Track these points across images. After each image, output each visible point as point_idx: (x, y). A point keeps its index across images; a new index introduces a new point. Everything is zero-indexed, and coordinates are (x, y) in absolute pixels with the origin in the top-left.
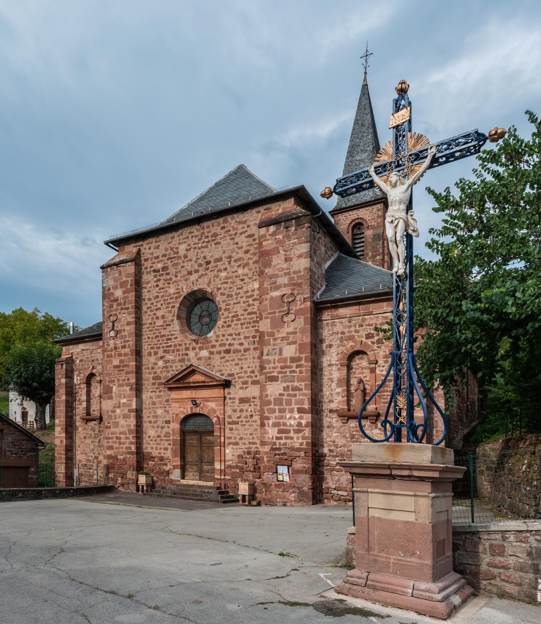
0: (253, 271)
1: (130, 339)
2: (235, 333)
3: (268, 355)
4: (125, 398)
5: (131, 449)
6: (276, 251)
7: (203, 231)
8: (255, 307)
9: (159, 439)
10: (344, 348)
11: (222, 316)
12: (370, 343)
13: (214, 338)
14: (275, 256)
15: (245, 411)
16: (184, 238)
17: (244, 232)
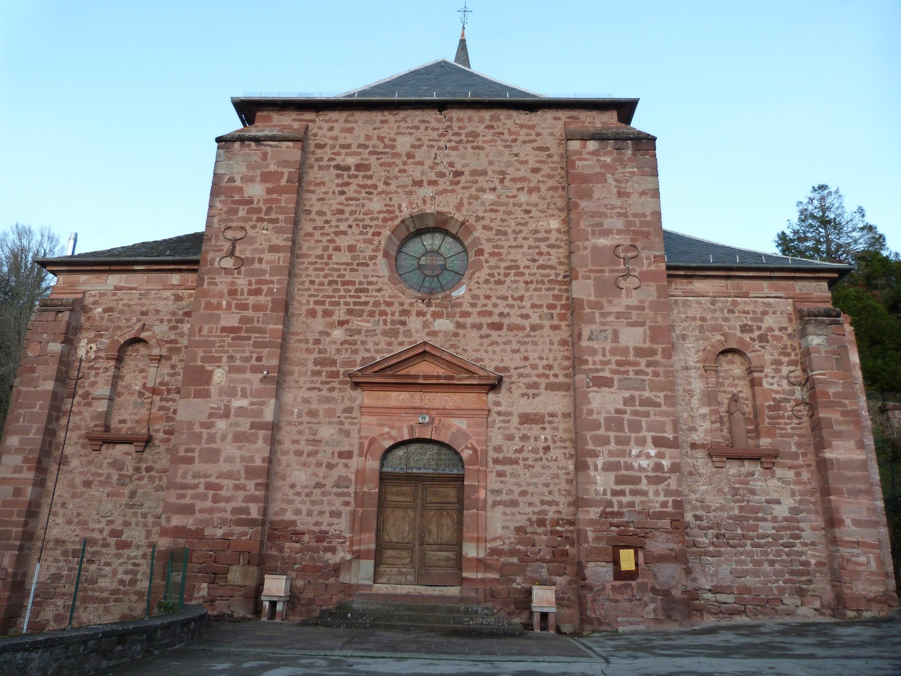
0: (548, 201)
1: (275, 279)
2: (512, 296)
3: (590, 339)
4: (244, 396)
5: (249, 513)
6: (600, 178)
7: (449, 123)
8: (553, 258)
9: (318, 491)
10: (706, 343)
11: (484, 264)
12: (748, 340)
13: (468, 299)
14: (600, 185)
15: (532, 439)
16: (408, 127)
17: (529, 142)
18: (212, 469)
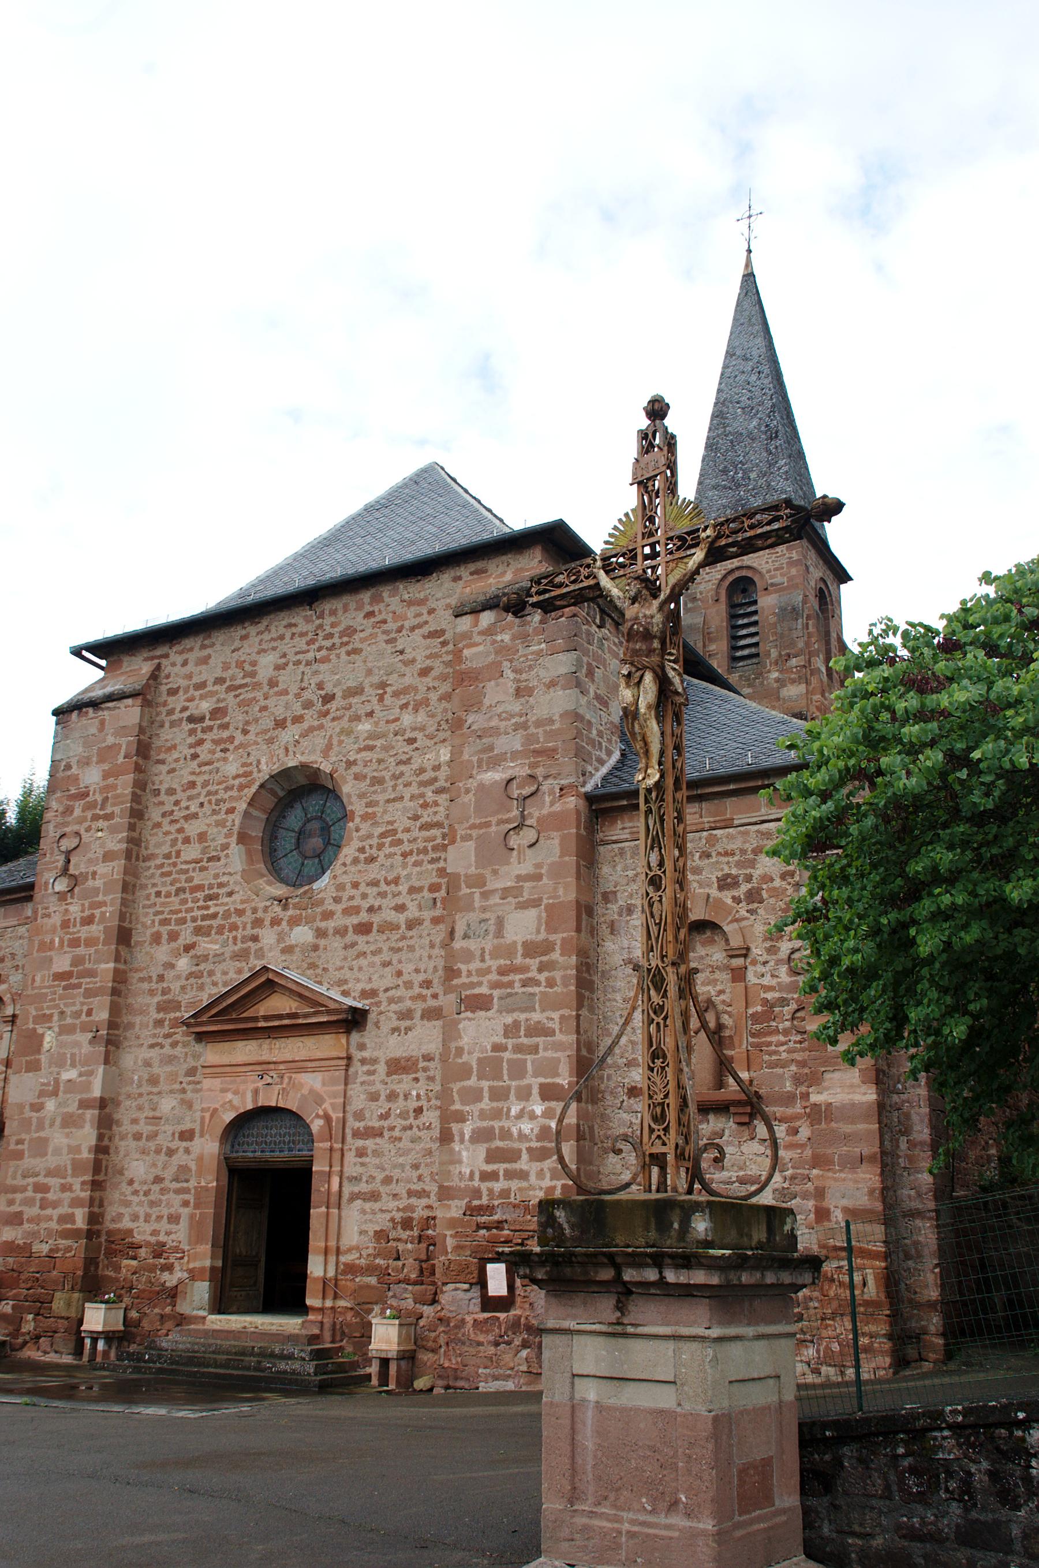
0: (439, 718)
1: (108, 898)
2: (386, 879)
3: (466, 936)
4: (73, 1065)
6: (495, 671)
9: (156, 1188)
11: (354, 833)
14: (493, 683)
16: (272, 639)
17: (419, 626)
18: (39, 1164)
